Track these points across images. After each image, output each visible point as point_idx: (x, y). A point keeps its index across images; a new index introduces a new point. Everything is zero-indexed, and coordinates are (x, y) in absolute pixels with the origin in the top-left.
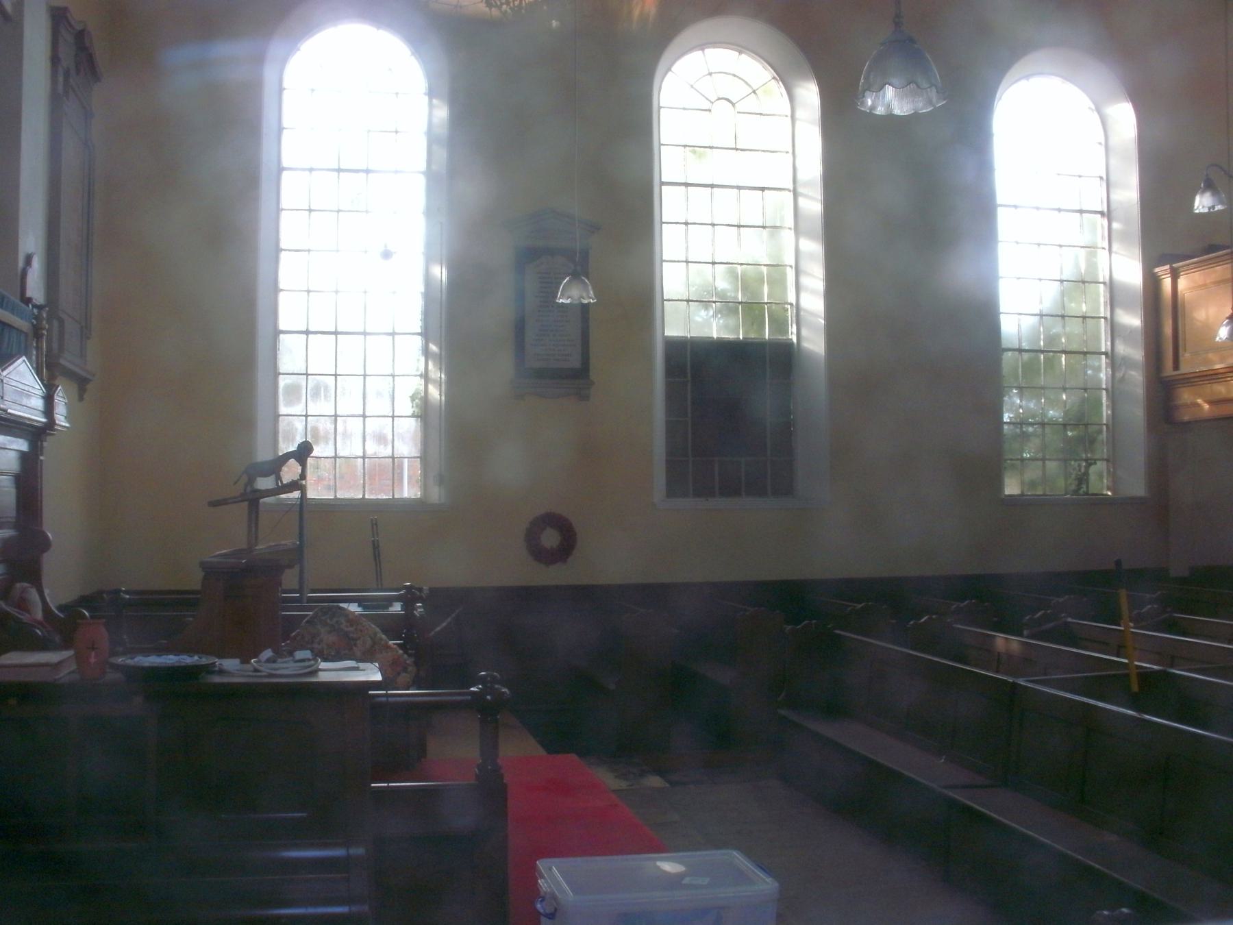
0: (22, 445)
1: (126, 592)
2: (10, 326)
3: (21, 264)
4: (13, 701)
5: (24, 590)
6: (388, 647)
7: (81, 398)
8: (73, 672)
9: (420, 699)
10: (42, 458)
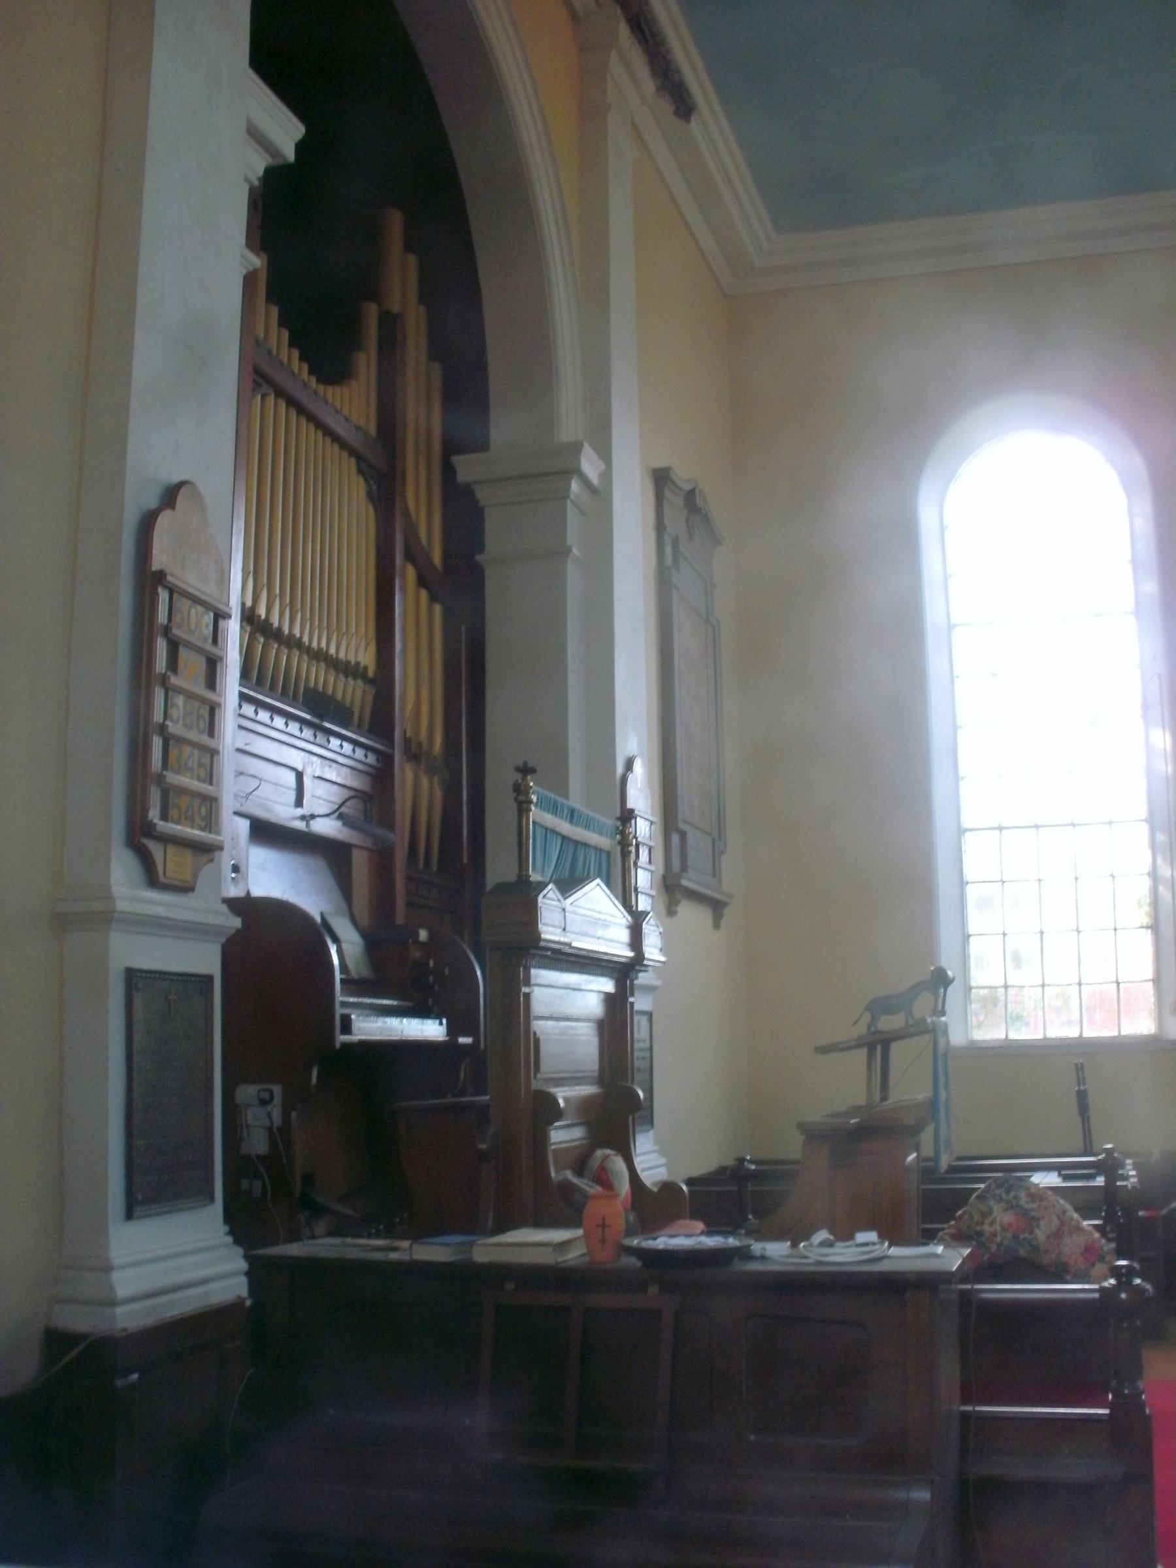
0: (607, 985)
1: (751, 1162)
2: (586, 845)
3: (620, 770)
4: (510, 1286)
5: (606, 1158)
6: (1079, 1228)
7: (717, 926)
8: (583, 1255)
9: (1082, 1296)
10: (631, 999)
